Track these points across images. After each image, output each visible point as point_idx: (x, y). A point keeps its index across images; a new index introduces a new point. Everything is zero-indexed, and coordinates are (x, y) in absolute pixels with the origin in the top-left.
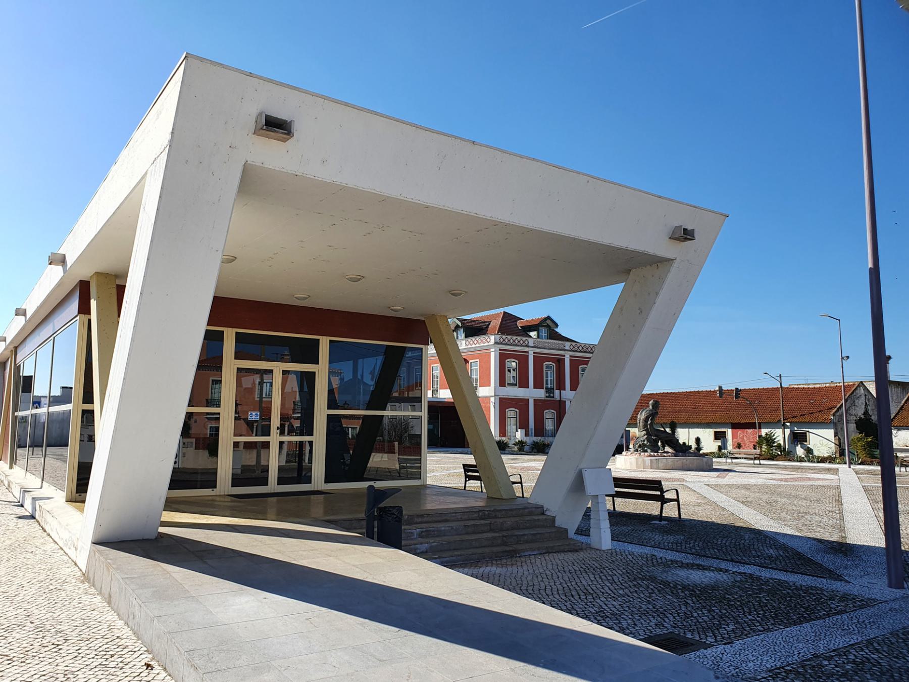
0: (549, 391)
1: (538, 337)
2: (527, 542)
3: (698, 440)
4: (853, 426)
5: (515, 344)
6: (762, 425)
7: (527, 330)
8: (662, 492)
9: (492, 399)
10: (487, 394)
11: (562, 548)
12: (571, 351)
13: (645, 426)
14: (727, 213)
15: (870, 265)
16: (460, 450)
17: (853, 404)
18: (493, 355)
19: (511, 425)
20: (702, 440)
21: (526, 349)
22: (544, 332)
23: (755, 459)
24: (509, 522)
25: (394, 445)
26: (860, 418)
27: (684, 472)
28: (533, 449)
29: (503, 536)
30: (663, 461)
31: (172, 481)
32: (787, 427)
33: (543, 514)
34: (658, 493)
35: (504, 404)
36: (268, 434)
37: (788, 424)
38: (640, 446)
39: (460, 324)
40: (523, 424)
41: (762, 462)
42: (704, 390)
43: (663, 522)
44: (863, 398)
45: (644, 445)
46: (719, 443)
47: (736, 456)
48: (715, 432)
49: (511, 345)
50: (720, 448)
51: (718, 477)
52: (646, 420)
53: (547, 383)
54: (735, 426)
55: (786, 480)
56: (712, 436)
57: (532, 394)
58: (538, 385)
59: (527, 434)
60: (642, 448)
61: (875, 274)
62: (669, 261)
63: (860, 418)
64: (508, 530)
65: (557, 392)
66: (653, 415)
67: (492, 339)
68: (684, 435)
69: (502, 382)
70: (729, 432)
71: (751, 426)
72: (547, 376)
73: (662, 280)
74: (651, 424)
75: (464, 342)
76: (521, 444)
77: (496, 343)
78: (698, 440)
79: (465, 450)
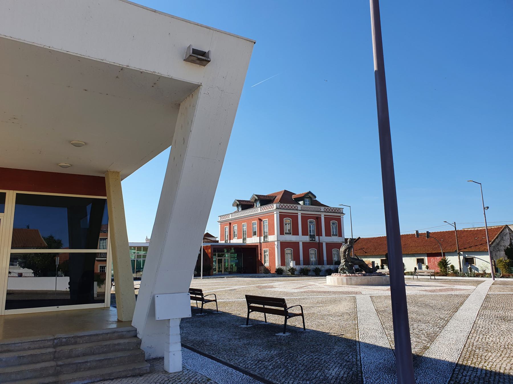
0: (312, 237)
1: (304, 204)
2: (90, 369)
4: (503, 253)
6: (446, 254)
8: (285, 306)
9: (276, 243)
10: (273, 240)
11: (123, 374)
12: (325, 212)
13: (344, 256)
14: (254, 39)
15: (375, 68)
17: (502, 239)
18: (275, 215)
19: (288, 257)
21: (296, 212)
22: (307, 201)
23: (432, 275)
24: (80, 348)
26: (507, 248)
28: (301, 273)
29: (57, 366)
31: (7, 301)
32: (461, 255)
33: (136, 336)
34: (283, 309)
35: (284, 245)
37: (462, 253)
38: (341, 270)
41: (436, 277)
43: (287, 334)
44: (508, 236)
49: (287, 209)
53: (310, 232)
54: (429, 255)
55: (434, 291)
57: (301, 239)
58: (305, 233)
59: (298, 263)
61: (380, 76)
62: (197, 87)
63: (507, 248)
64: (78, 356)
65: (317, 237)
66: (349, 249)
68: (368, 261)
70: (426, 259)
71: (439, 254)
72: (310, 228)
75: (259, 209)
77: (277, 208)
79: (257, 275)
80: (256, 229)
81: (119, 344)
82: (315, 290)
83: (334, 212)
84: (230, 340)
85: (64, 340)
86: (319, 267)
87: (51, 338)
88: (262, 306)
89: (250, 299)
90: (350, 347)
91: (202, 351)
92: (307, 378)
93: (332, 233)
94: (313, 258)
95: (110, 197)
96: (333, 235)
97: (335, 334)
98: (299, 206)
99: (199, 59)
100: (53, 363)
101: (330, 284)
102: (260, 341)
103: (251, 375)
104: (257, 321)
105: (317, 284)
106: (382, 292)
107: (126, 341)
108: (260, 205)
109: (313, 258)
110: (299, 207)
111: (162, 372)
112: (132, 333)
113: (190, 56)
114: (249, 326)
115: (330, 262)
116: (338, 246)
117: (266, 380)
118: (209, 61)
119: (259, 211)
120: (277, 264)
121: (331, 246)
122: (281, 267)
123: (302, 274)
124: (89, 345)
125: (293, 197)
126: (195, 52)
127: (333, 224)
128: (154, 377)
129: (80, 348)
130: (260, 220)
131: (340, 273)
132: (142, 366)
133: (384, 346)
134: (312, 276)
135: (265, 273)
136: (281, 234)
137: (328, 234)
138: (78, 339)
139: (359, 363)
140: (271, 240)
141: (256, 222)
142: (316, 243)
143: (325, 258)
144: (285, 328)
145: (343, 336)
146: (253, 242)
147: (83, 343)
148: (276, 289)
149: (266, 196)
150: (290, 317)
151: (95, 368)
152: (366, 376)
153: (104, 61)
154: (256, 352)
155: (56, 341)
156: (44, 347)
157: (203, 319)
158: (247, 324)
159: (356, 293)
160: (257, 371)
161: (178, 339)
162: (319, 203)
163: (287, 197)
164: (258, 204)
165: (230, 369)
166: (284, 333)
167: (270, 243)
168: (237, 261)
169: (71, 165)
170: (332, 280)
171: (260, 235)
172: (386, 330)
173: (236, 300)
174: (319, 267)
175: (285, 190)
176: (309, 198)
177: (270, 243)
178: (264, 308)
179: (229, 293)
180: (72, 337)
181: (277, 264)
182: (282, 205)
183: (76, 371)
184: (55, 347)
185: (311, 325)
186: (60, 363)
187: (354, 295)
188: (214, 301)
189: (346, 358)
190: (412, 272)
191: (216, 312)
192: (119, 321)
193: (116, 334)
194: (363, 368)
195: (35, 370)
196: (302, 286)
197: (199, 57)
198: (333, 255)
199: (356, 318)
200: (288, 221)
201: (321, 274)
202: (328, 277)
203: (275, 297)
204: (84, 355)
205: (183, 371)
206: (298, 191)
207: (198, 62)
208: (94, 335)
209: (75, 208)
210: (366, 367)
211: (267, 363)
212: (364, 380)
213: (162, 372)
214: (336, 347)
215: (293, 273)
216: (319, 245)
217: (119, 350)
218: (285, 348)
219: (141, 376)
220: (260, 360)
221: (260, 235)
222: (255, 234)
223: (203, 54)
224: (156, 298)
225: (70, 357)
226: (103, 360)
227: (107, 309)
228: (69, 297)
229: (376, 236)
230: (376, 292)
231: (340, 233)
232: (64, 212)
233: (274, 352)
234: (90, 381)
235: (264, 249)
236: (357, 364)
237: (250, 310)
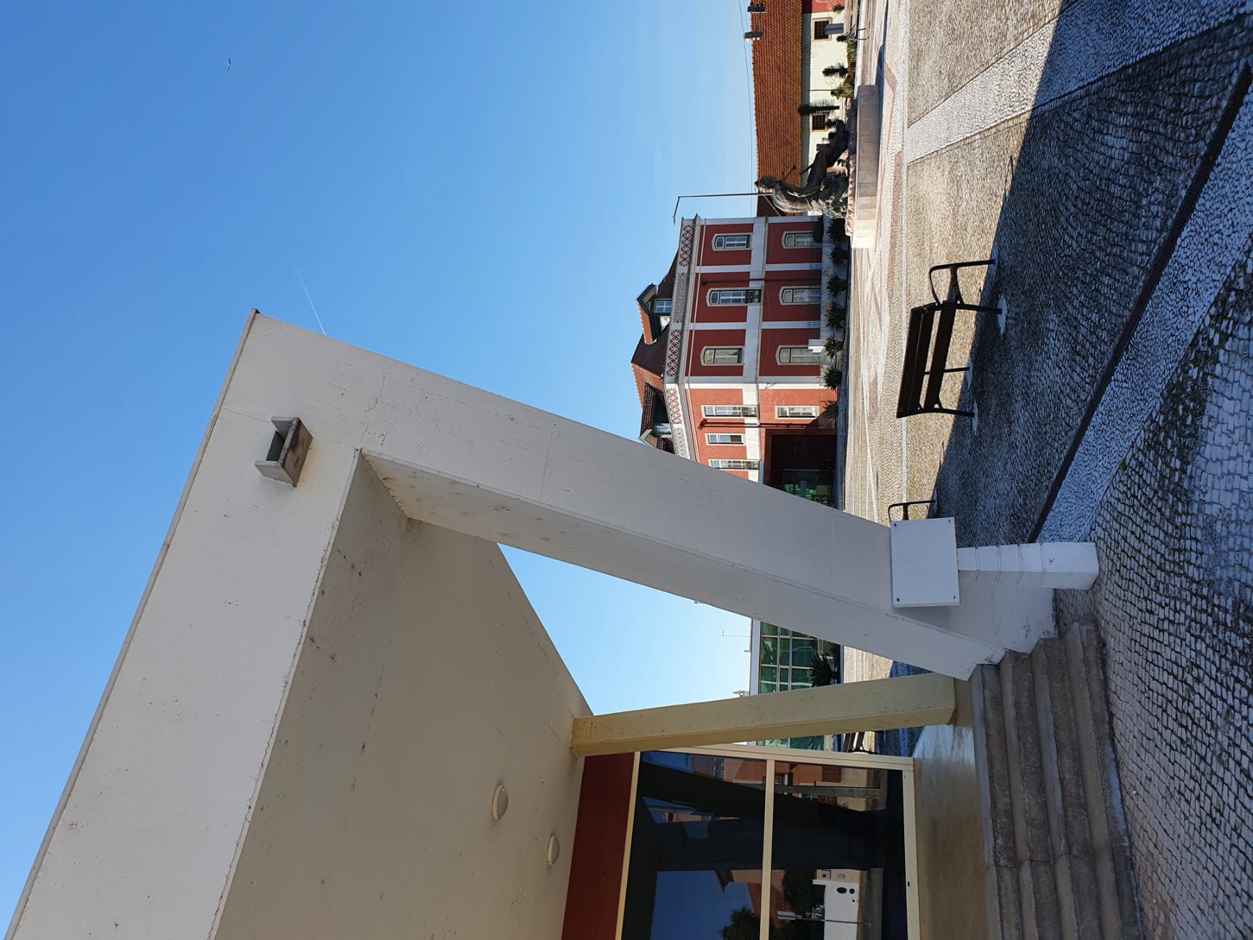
1: (668, 314)
2: (1080, 774)
3: (828, 72)
7: (657, 331)
8: (931, 308)
9: (762, 386)
10: (755, 393)
11: (1096, 687)
12: (690, 264)
13: (802, 201)
16: (840, 448)
18: (693, 386)
20: (827, 66)
22: (661, 306)
24: (1024, 800)
28: (839, 327)
33: (997, 667)
34: (938, 314)
35: (769, 368)
36: (819, 260)
38: (837, 210)
40: (802, 338)
42: (751, 54)
43: (1003, 304)
47: (854, 22)
49: (679, 357)
51: (893, 89)
52: (793, 200)
53: (739, 301)
56: (822, 42)
57: (754, 324)
58: (741, 315)
59: (816, 334)
64: (1045, 806)
65: (752, 285)
66: (785, 190)
67: (670, 387)
69: (735, 371)
70: (816, 16)
72: (728, 301)
73: (415, 474)
74: (800, 191)
75: (675, 426)
76: (832, 347)
77: (676, 381)
78: (828, 72)
79: (840, 433)
80: (727, 434)
81: (1017, 705)
82: (885, 272)
83: (692, 242)
84: (1013, 446)
85: (1000, 841)
86: (825, 280)
87: (995, 873)
88: (926, 378)
89: (907, 406)
90: (1046, 127)
91: (1039, 511)
92: (1133, 208)
93: (744, 248)
94: (804, 296)
95: (635, 743)
96: (748, 245)
97: (1010, 178)
98: (672, 328)
99: (293, 447)
100: (1062, 866)
101: (873, 239)
102: (1019, 369)
103: (1115, 360)
104: (962, 392)
105: (870, 273)
106: (898, 101)
107: (1009, 687)
108: (666, 425)
109: (804, 296)
110: (676, 326)
111: (1094, 594)
112: (989, 675)
113: (283, 465)
114: (976, 411)
115: (815, 255)
116: (775, 233)
117: (1132, 317)
118: (299, 422)
119: (682, 426)
120: (816, 385)
121: (775, 253)
122: (823, 374)
123: (842, 323)
124: (1016, 777)
125: (649, 341)
126: (274, 454)
127: (720, 244)
128: (1109, 610)
129: (1024, 800)
130: (704, 424)
131: (844, 214)
132: (1079, 642)
133: (1049, 40)
134: (847, 298)
135: (836, 415)
136: (741, 374)
137: (745, 257)
138: (1000, 806)
139: (1094, 87)
140: (755, 398)
141: (707, 435)
142: (766, 286)
143: (805, 266)
144: (987, 311)
145: (1016, 155)
146: (757, 443)
147: (1010, 796)
148: (881, 371)
149: (645, 408)
150: (959, 297)
151: (1078, 759)
152: (1134, 53)
153: (290, 682)
154: (1050, 372)
155: (1002, 862)
156: (1018, 891)
157: (959, 499)
158: (971, 415)
159: (898, 165)
160: (1104, 348)
161: (1009, 551)
162: (667, 277)
163: (650, 356)
164: (664, 428)
165: (1096, 420)
166: (1000, 311)
167: (762, 400)
168: (803, 483)
169: (553, 834)
170: (864, 235)
171: (742, 425)
172: (1005, 51)
173: (904, 463)
174: (825, 280)
175: (633, 361)
176: (653, 301)
177: (762, 400)
178: (932, 373)
179: (890, 461)
180: (994, 821)
181: (816, 385)
182: (667, 369)
183: (1085, 806)
184: (1016, 864)
185: (982, 247)
186: (1061, 846)
187: (904, 170)
188: (906, 511)
189: (1078, 126)
190: (849, 46)
191: (935, 505)
192: (954, 720)
193: (991, 715)
194: (1111, 70)
195: (1079, 910)
196: (873, 307)
197: (289, 447)
198: (797, 302)
199: (967, 142)
200: (709, 356)
201: (843, 277)
202: (855, 244)
203: (901, 368)
204: (1041, 789)
205: (1087, 592)
206: (635, 328)
207: (299, 450)
208: (991, 767)
209: (662, 848)
210: (1107, 64)
211: (1083, 330)
212: (1145, 54)
213: (1094, 594)
214: (1045, 164)
215: (839, 346)
216: (773, 280)
217: (1033, 705)
218: (1042, 297)
219: (1104, 645)
220: (1074, 349)
221: (742, 425)
222: (737, 439)
223: (279, 438)
224: (903, 603)
225: (1046, 826)
226: (1057, 741)
227: (918, 768)
228: (878, 873)
229: (755, 159)
230: (898, 115)
231: (745, 228)
232: (667, 881)
233: (1053, 321)
234: (1113, 769)
235: (776, 418)
236: (1100, 89)
237: (936, 406)
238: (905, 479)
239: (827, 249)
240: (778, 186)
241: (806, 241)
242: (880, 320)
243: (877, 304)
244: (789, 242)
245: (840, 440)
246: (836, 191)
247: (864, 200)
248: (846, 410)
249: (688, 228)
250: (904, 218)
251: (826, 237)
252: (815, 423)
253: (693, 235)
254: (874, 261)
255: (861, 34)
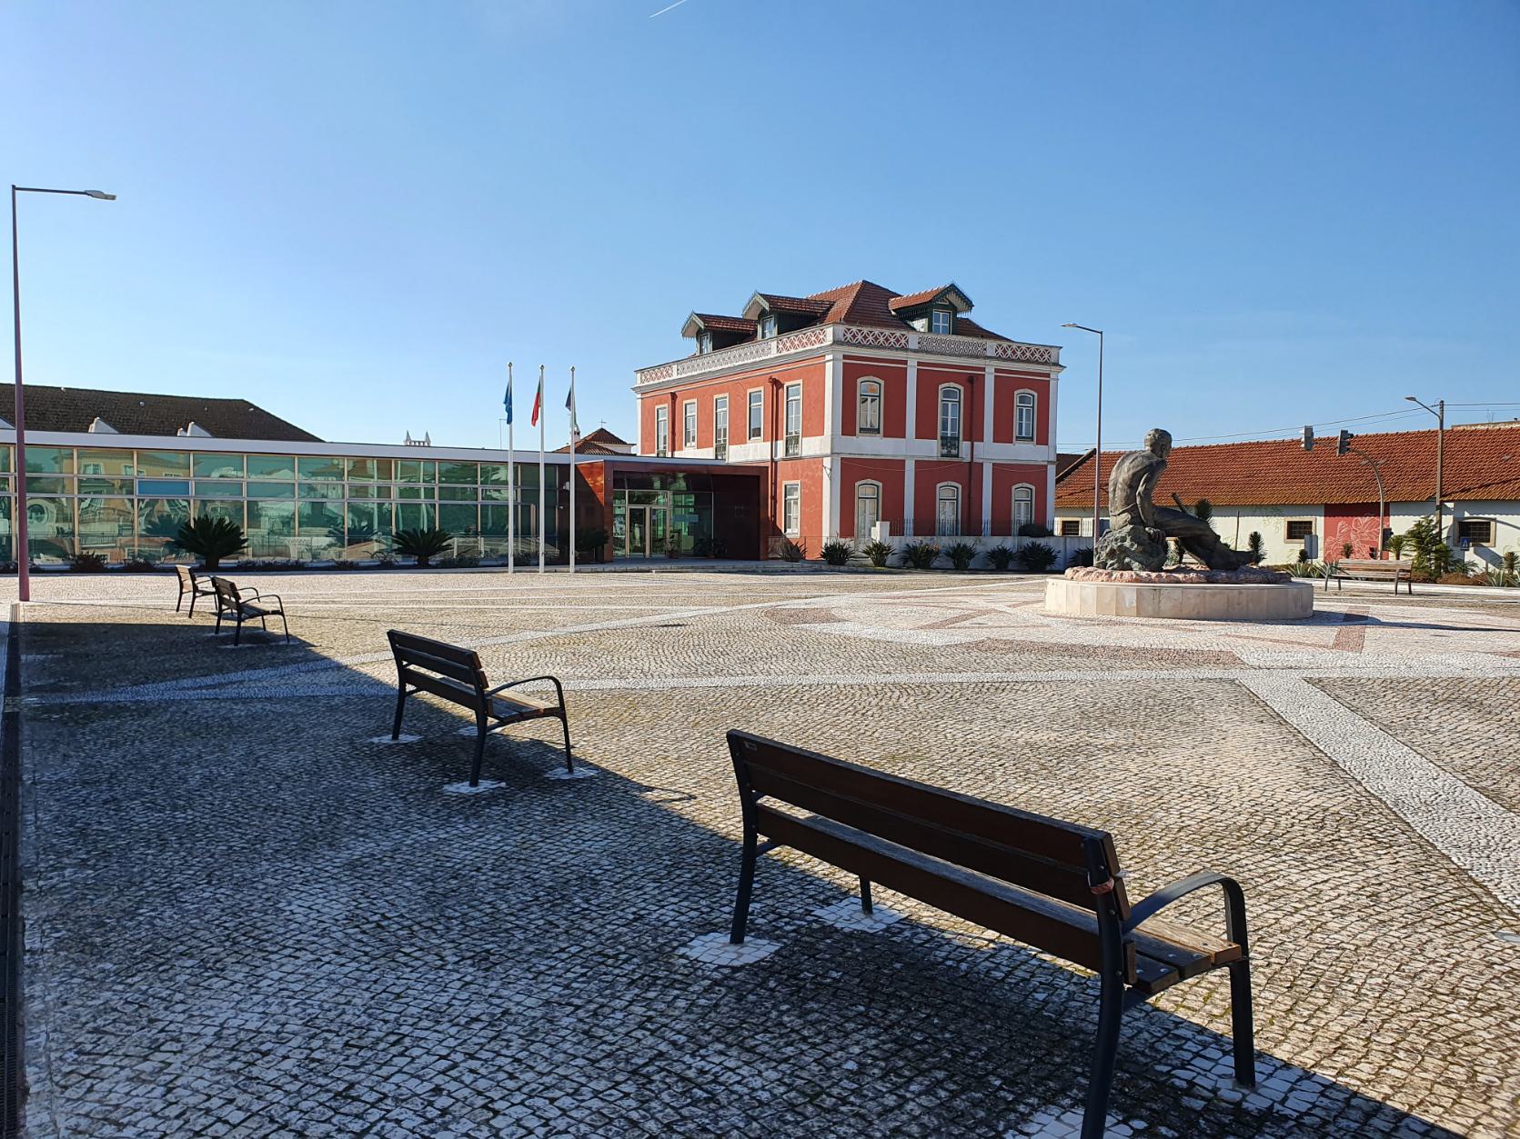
1: (930, 329)
3: (1255, 539)
5: (877, 345)
9: (827, 462)
12: (999, 358)
13: (1129, 499)
16: (740, 565)
18: (829, 366)
19: (866, 508)
20: (1264, 538)
21: (901, 355)
22: (942, 320)
25: (1166, 546)
27: (1232, 628)
28: (905, 560)
30: (1173, 593)
32: (1448, 512)
35: (852, 470)
38: (1112, 554)
39: (767, 306)
40: (891, 513)
41: (1416, 588)
42: (1270, 440)
45: (1124, 551)
46: (1299, 546)
47: (1352, 574)
48: (1290, 523)
50: (1304, 556)
52: (1132, 484)
53: (945, 428)
54: (1332, 511)
58: (925, 431)
59: (897, 530)
60: (1119, 558)
65: (965, 446)
67: (829, 333)
68: (1230, 530)
69: (849, 425)
70: (1319, 523)
71: (1370, 509)
72: (945, 413)
76: (879, 552)
77: (836, 342)
78: (1255, 539)
79: (761, 564)
80: (762, 421)
86: (969, 541)
93: (1016, 433)
94: (947, 512)
98: (910, 335)
108: (775, 331)
109: (947, 512)
115: (1001, 527)
116: (1034, 474)
119: (774, 353)
120: (828, 532)
121: (1007, 475)
122: (842, 541)
123: (910, 563)
125: (893, 304)
127: (1022, 399)
130: (777, 384)
131: (1104, 565)
134: (945, 570)
135: (786, 560)
143: (987, 514)
148: (850, 629)
163: (870, 305)
164: (771, 329)
168: (695, 519)
170: (1064, 598)
171: (775, 437)
174: (969, 541)
175: (865, 282)
181: (828, 532)
182: (854, 329)
206: (908, 285)
215: (880, 559)
221: (775, 437)
222: (756, 432)
235: (783, 483)
238: (653, 684)
239: (1010, 543)
240: (1156, 459)
241: (1020, 514)
242: (932, 627)
243: (955, 620)
244: (1020, 493)
245: (753, 564)
246: (1144, 552)
247: (1130, 596)
248: (794, 572)
249: (1046, 357)
250: (1135, 674)
251: (1027, 541)
252: (777, 533)
253: (1037, 362)
254: (1024, 613)
255: (1333, 584)
